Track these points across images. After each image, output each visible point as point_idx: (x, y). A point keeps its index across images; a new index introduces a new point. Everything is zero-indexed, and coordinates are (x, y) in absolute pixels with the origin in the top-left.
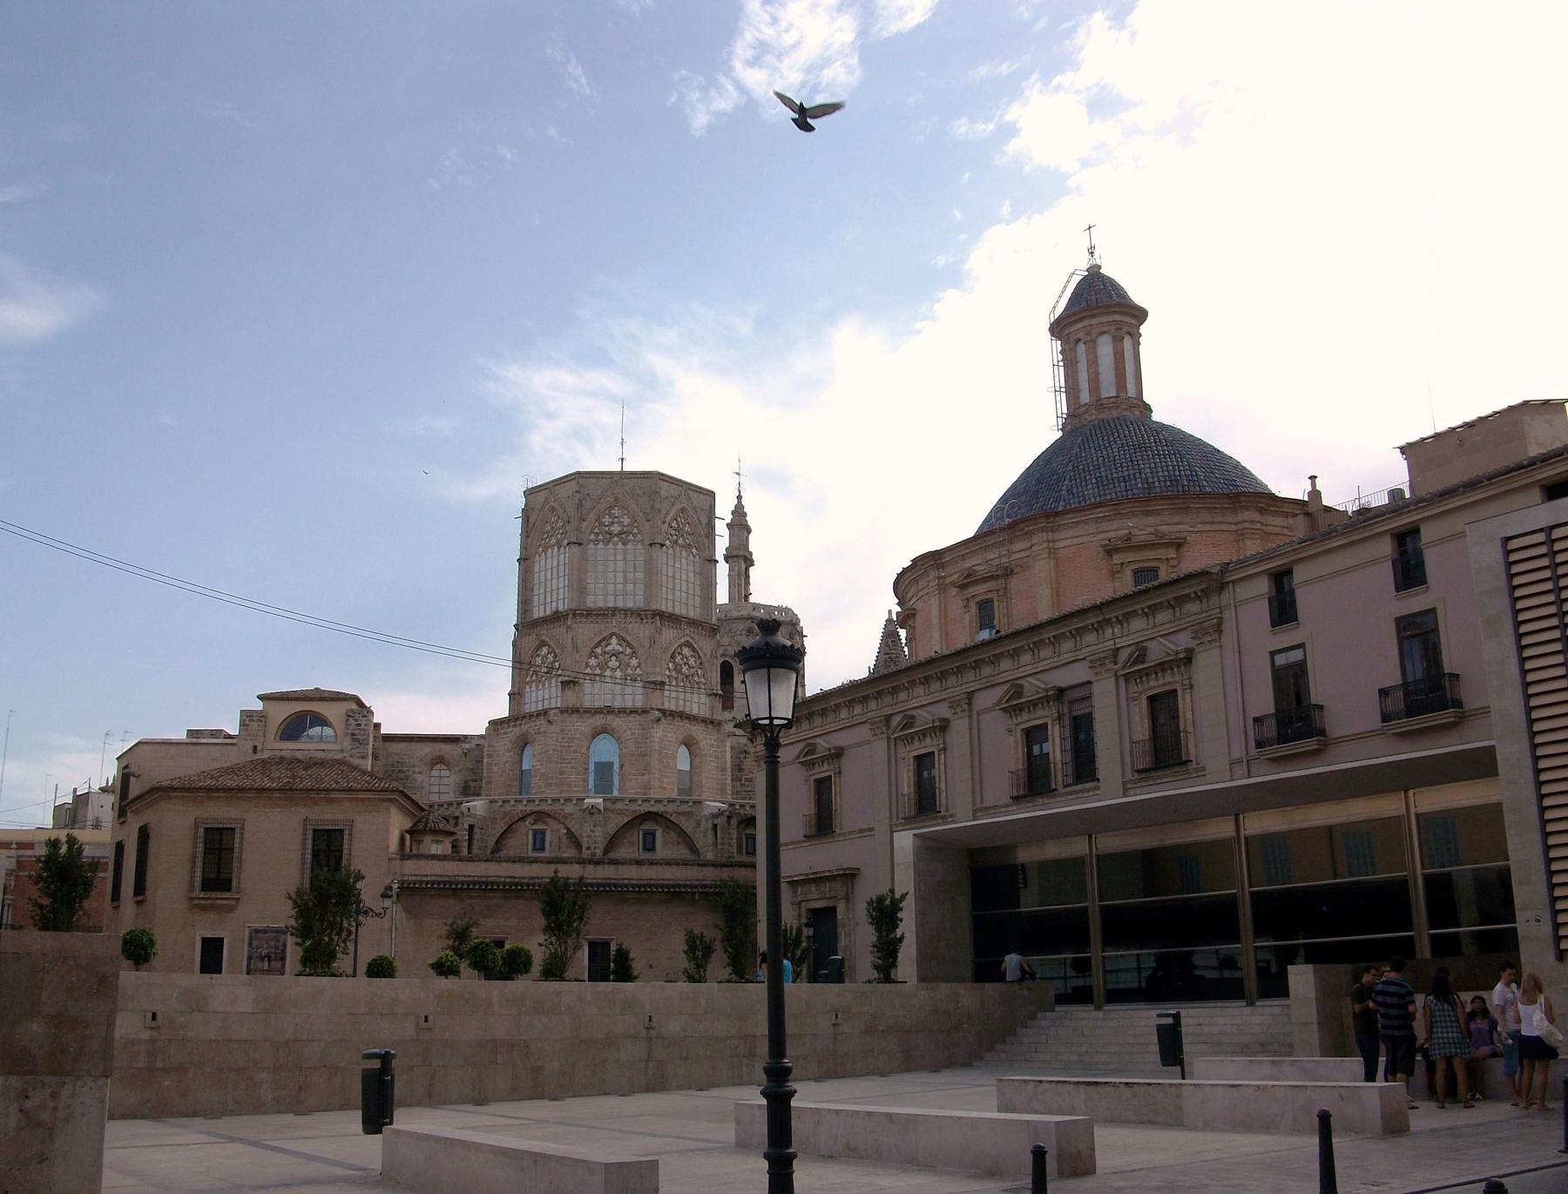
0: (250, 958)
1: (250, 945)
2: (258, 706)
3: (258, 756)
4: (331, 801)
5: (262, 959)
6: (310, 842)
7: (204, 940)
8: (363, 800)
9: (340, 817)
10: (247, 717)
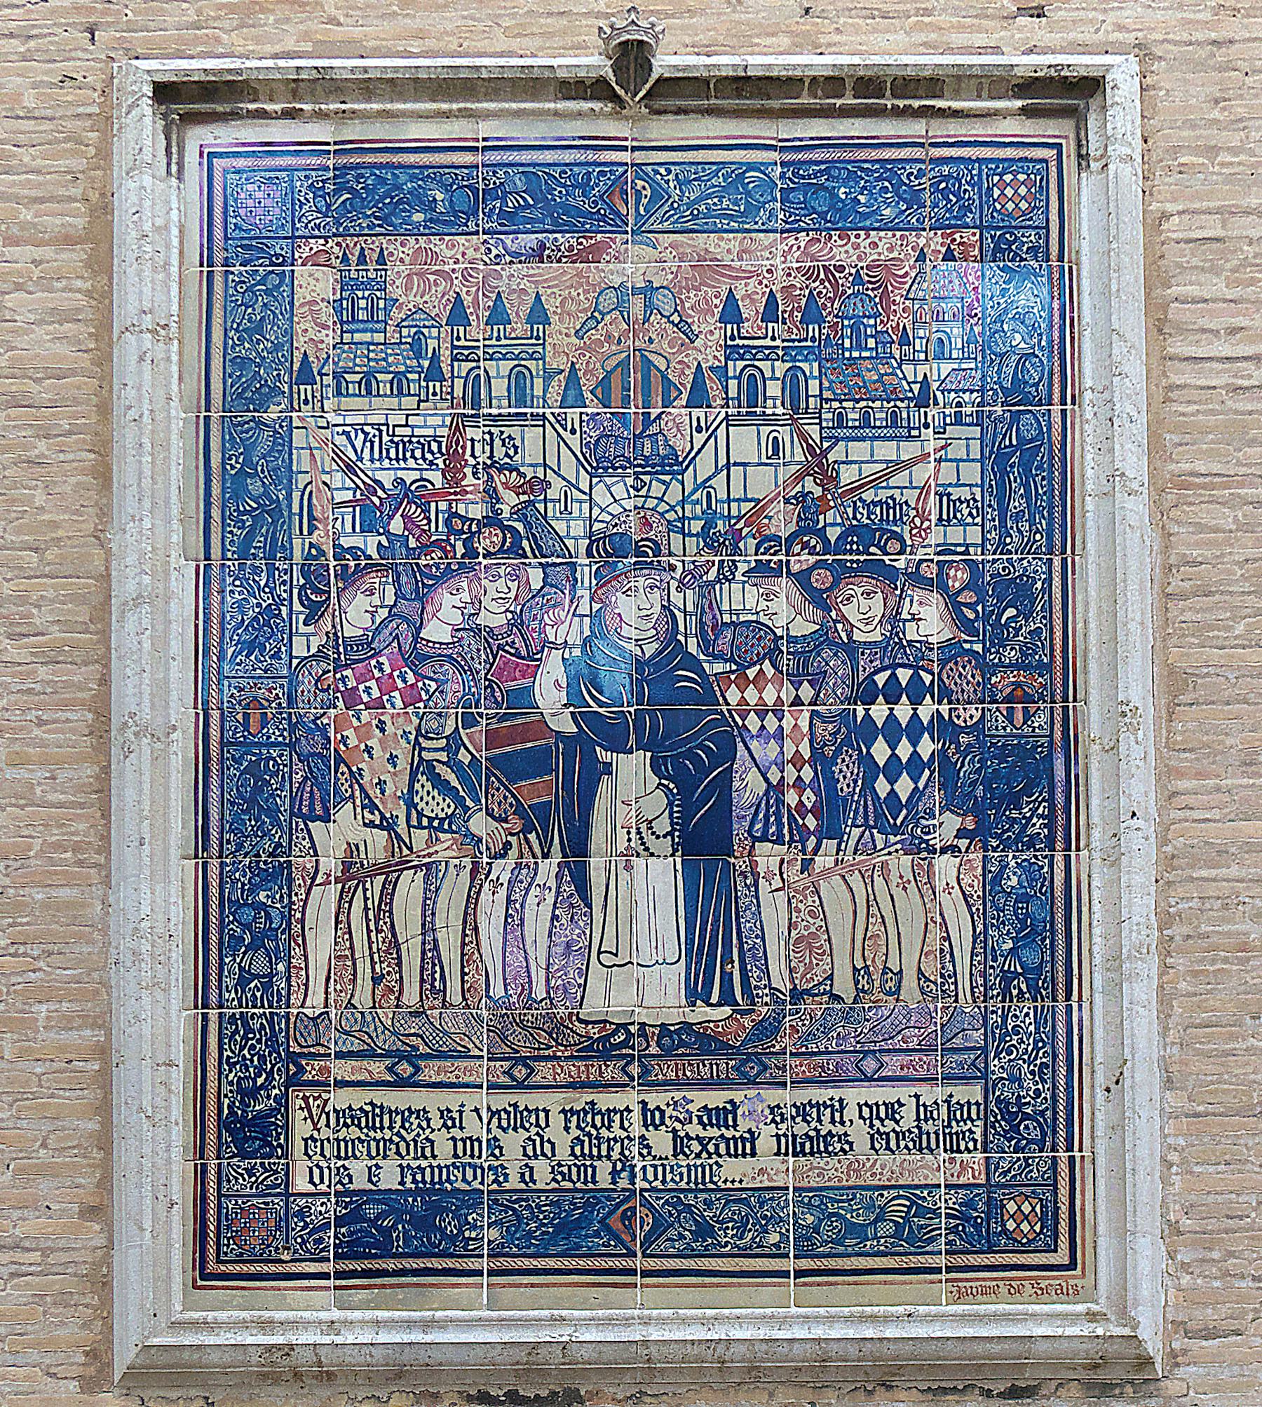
5: (539, 788)
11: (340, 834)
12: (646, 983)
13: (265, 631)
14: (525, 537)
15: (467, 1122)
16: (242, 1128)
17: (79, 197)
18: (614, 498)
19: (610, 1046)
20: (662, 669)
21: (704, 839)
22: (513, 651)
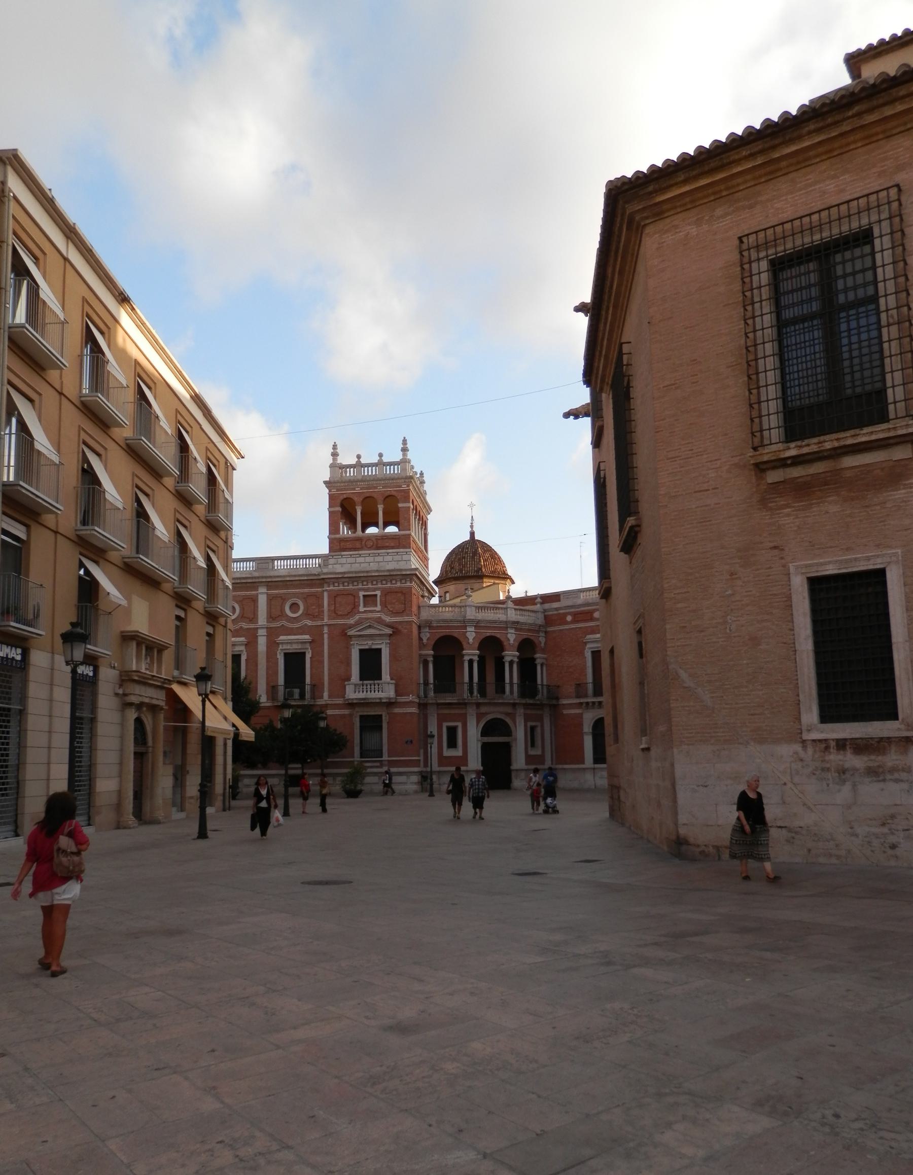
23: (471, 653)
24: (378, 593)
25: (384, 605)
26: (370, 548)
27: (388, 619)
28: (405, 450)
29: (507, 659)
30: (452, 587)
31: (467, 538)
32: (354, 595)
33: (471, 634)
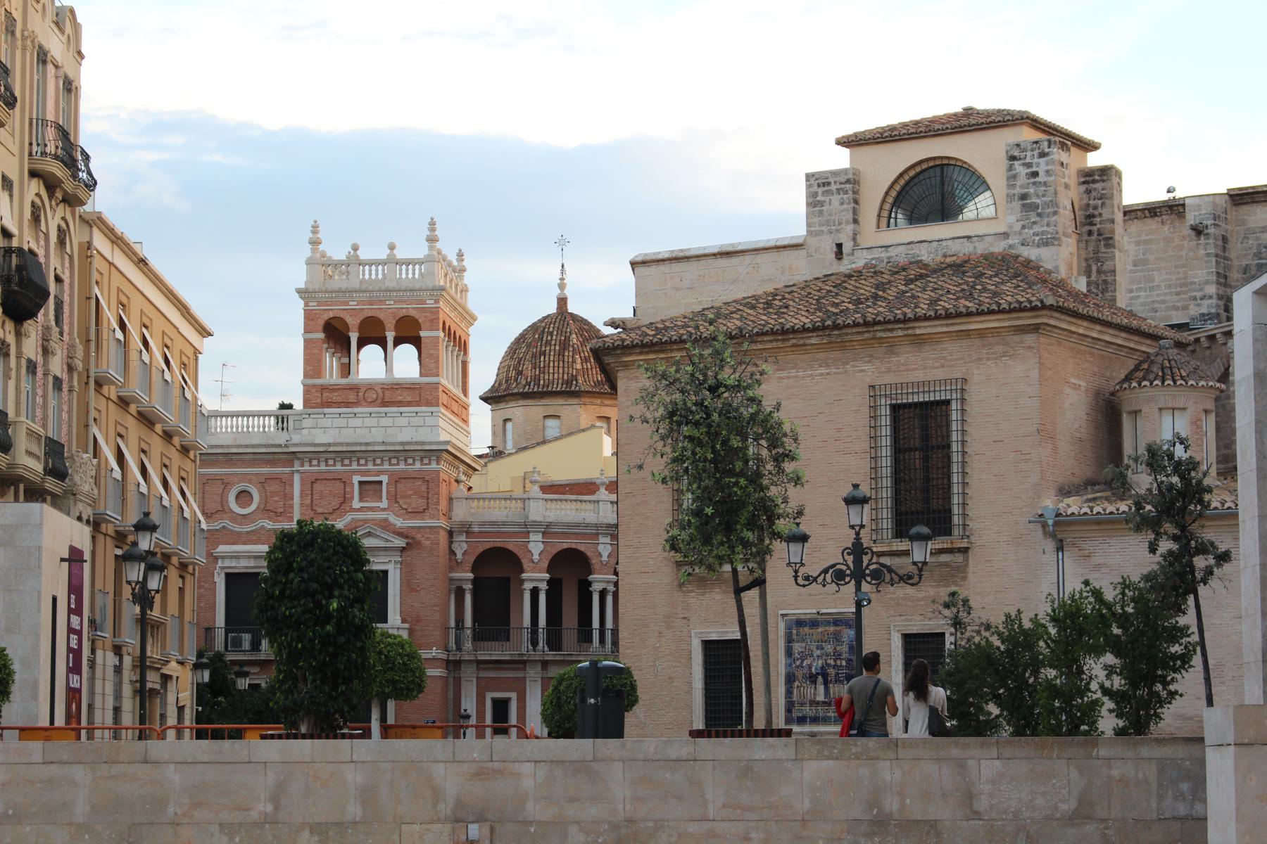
0: (790, 679)
1: (789, 652)
2: (841, 159)
3: (845, 267)
4: (919, 341)
5: (812, 679)
6: (886, 431)
7: (708, 645)
8: (981, 334)
9: (940, 374)
10: (819, 184)
11: (796, 683)
12: (821, 698)
13: (790, 665)
14: (811, 655)
15: (808, 711)
16: (789, 710)
17: (861, 321)
18: (819, 652)
19: (818, 703)
20: (822, 668)
21: (826, 683)
22: (810, 667)
23: (535, 577)
24: (384, 478)
25: (394, 498)
26: (372, 403)
27: (399, 522)
28: (432, 240)
29: (597, 587)
30: (519, 412)
31: (552, 308)
32: (345, 482)
33: (536, 547)
